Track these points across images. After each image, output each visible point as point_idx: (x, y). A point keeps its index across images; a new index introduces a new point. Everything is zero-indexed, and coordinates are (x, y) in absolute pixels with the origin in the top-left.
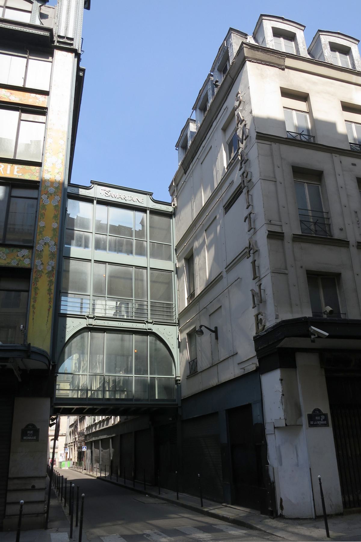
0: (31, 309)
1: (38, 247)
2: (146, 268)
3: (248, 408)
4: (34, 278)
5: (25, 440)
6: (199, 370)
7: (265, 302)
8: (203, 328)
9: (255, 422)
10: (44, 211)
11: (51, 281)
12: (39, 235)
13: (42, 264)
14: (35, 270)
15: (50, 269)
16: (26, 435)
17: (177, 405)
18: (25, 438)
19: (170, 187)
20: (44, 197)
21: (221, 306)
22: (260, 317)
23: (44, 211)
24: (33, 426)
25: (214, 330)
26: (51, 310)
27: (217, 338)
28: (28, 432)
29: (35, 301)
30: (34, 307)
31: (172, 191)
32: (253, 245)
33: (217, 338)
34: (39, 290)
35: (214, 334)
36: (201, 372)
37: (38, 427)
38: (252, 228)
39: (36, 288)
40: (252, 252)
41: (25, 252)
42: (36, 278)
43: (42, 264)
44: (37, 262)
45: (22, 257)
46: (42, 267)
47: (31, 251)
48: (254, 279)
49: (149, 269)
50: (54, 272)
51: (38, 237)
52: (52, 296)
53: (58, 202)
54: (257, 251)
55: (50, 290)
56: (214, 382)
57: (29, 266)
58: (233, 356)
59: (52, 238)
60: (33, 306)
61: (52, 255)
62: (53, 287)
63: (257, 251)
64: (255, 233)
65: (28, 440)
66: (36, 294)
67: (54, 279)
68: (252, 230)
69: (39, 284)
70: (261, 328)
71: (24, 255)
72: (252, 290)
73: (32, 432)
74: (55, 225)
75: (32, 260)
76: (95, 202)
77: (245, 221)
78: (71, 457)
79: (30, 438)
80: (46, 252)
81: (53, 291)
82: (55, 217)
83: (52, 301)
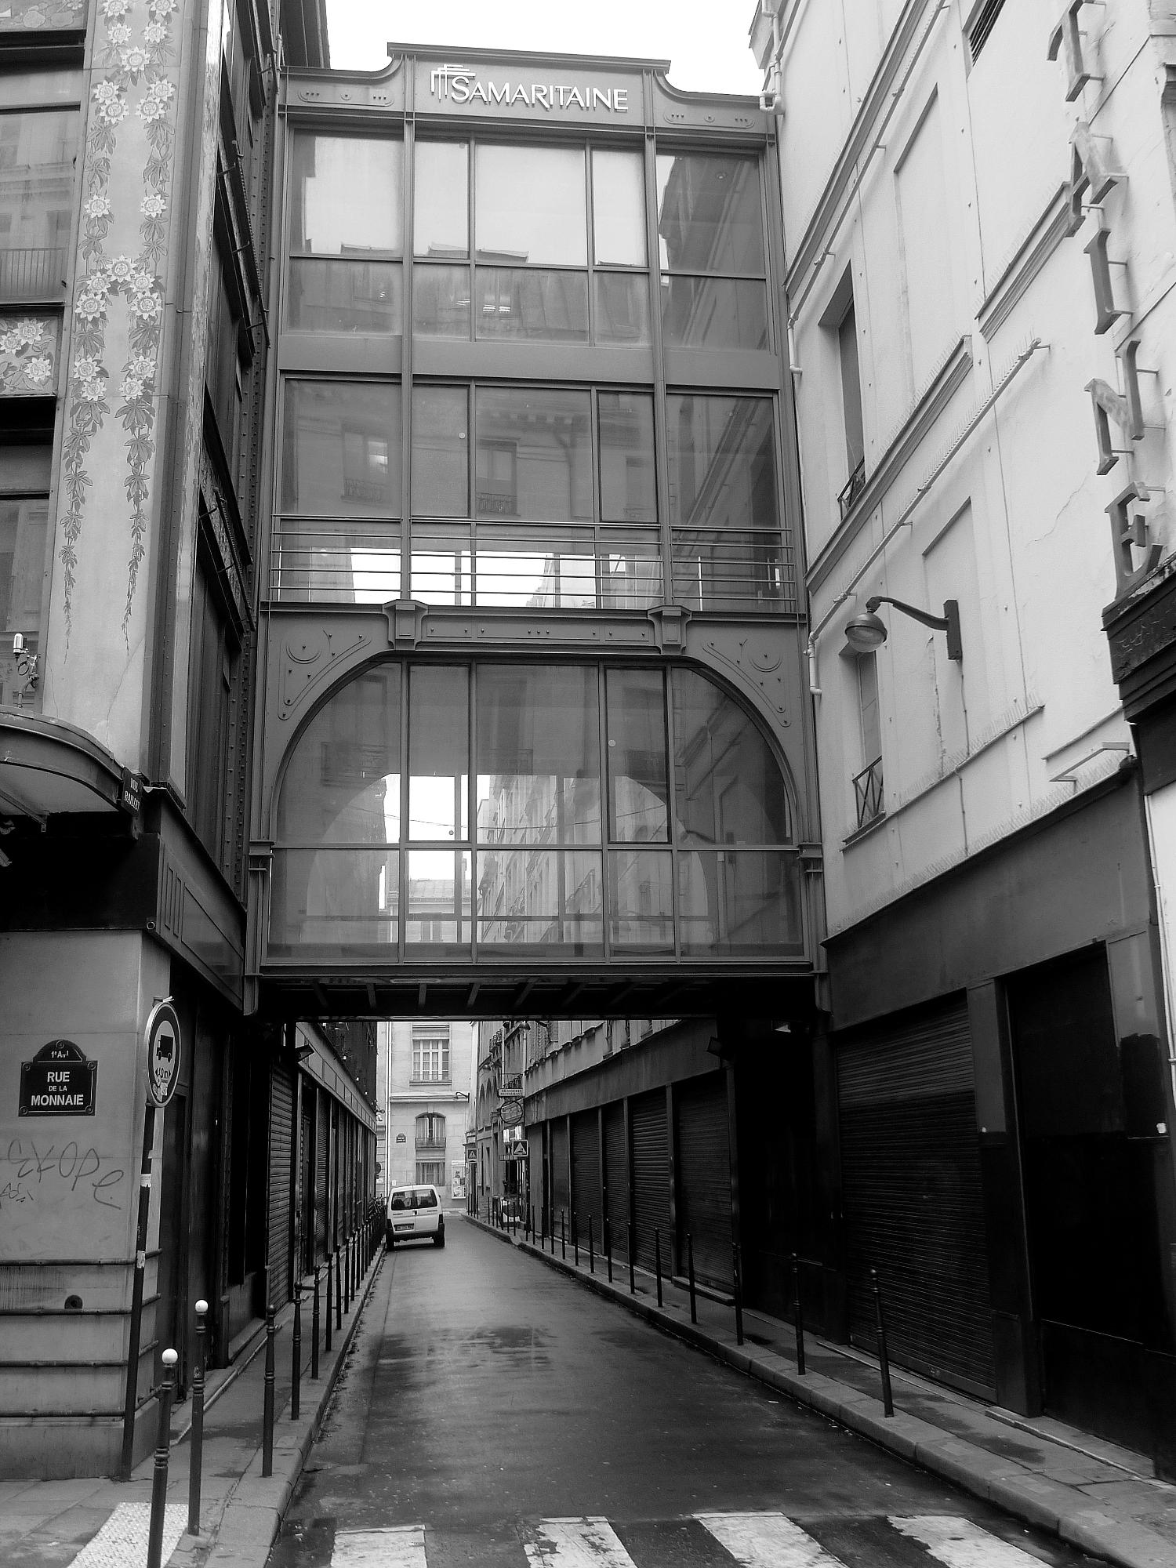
0: (60, 567)
1: (82, 306)
2: (648, 389)
3: (1090, 963)
4: (68, 434)
5: (37, 1107)
6: (890, 806)
7: (1163, 430)
8: (885, 612)
9: (1123, 1030)
10: (102, 153)
11: (139, 444)
12: (86, 255)
13: (103, 373)
14: (71, 402)
15: (138, 392)
16: (43, 1090)
17: (810, 967)
18: (36, 1100)
19: (753, 31)
20: (104, 92)
21: (968, 503)
22: (1134, 509)
23: (102, 153)
24: (70, 1048)
25: (939, 613)
26: (144, 564)
27: (956, 653)
28: (51, 1076)
29: (73, 534)
30: (69, 558)
31: (762, 44)
32: (1091, 163)
33: (956, 653)
34: (89, 483)
35: (941, 635)
36: (897, 814)
37: (90, 1057)
38: (1084, 79)
39: (79, 478)
40: (1087, 196)
41: (30, 331)
42: (78, 436)
43: (103, 373)
44: (82, 367)
45: (19, 353)
46: (101, 387)
47: (54, 324)
48: (1102, 329)
49: (660, 391)
50: (155, 401)
51: (81, 261)
52: (147, 504)
53: (166, 106)
54: (1111, 183)
55: (136, 479)
56: (949, 853)
57: (47, 391)
58: (1023, 722)
59: (143, 259)
60: (67, 551)
61: (145, 331)
62: (151, 468)
63: (1111, 183)
64: (1104, 103)
65: (53, 1107)
66: (78, 501)
67: (153, 432)
68: (1091, 87)
69: (90, 461)
70: (1139, 556)
71: (26, 347)
72: (1093, 387)
73: (65, 1076)
74: (155, 205)
75: (55, 361)
76: (409, 133)
77: (1053, 55)
78: (487, 1184)
79: (57, 1100)
80: (118, 327)
81: (149, 485)
82: (155, 168)
83: (147, 524)
